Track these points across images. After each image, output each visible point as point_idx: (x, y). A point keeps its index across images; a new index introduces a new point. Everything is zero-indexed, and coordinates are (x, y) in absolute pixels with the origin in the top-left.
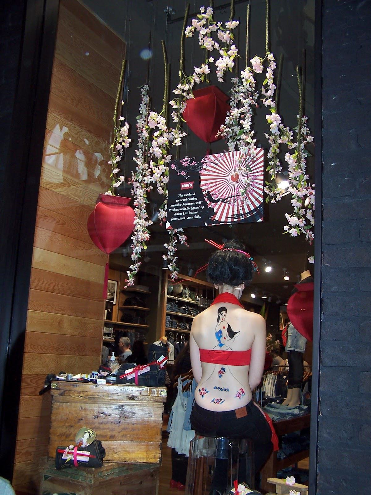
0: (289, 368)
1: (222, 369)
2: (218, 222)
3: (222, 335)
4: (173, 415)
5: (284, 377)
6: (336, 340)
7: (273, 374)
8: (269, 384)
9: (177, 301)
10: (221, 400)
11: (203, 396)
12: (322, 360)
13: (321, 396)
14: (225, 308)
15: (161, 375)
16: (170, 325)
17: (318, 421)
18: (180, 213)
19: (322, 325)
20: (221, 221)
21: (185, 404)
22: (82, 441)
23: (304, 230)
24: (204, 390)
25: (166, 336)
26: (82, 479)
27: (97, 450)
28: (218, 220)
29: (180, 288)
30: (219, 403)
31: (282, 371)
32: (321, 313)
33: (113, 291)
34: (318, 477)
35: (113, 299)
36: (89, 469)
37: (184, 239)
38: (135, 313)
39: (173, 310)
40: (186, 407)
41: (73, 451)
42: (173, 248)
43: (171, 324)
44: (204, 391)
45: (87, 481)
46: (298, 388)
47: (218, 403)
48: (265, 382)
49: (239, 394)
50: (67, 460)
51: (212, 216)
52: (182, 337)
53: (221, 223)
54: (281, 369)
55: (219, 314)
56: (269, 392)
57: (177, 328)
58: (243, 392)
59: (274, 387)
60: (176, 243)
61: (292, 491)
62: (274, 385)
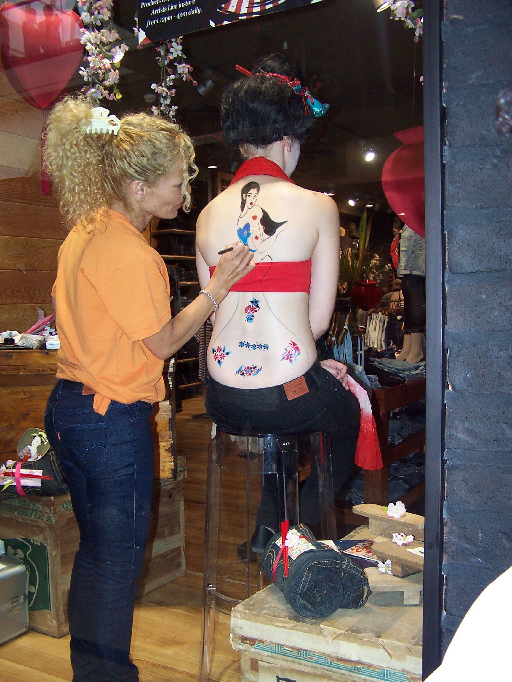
0: (405, 304)
2: (236, 15)
5: (398, 317)
6: (481, 207)
7: (380, 313)
8: (375, 330)
10: (254, 368)
11: (219, 362)
12: (448, 259)
13: (449, 344)
14: (251, 182)
17: (444, 405)
18: (162, 8)
19: (447, 173)
20: (241, 13)
22: (29, 452)
23: (411, 21)
24: (222, 350)
26: (36, 516)
27: (55, 466)
28: (234, 11)
30: (252, 373)
31: (394, 308)
32: (443, 143)
34: (446, 530)
36: (45, 499)
37: (186, 71)
38: (176, 239)
41: (14, 471)
42: (165, 89)
44: (222, 352)
45: (45, 519)
46: (419, 332)
47: (250, 374)
48: (369, 326)
49: (289, 352)
50: (4, 485)
51: (223, 6)
53: (240, 18)
54: (393, 306)
56: (376, 341)
58: (297, 349)
59: (384, 334)
60: (174, 80)
61: (397, 534)
62: (383, 330)
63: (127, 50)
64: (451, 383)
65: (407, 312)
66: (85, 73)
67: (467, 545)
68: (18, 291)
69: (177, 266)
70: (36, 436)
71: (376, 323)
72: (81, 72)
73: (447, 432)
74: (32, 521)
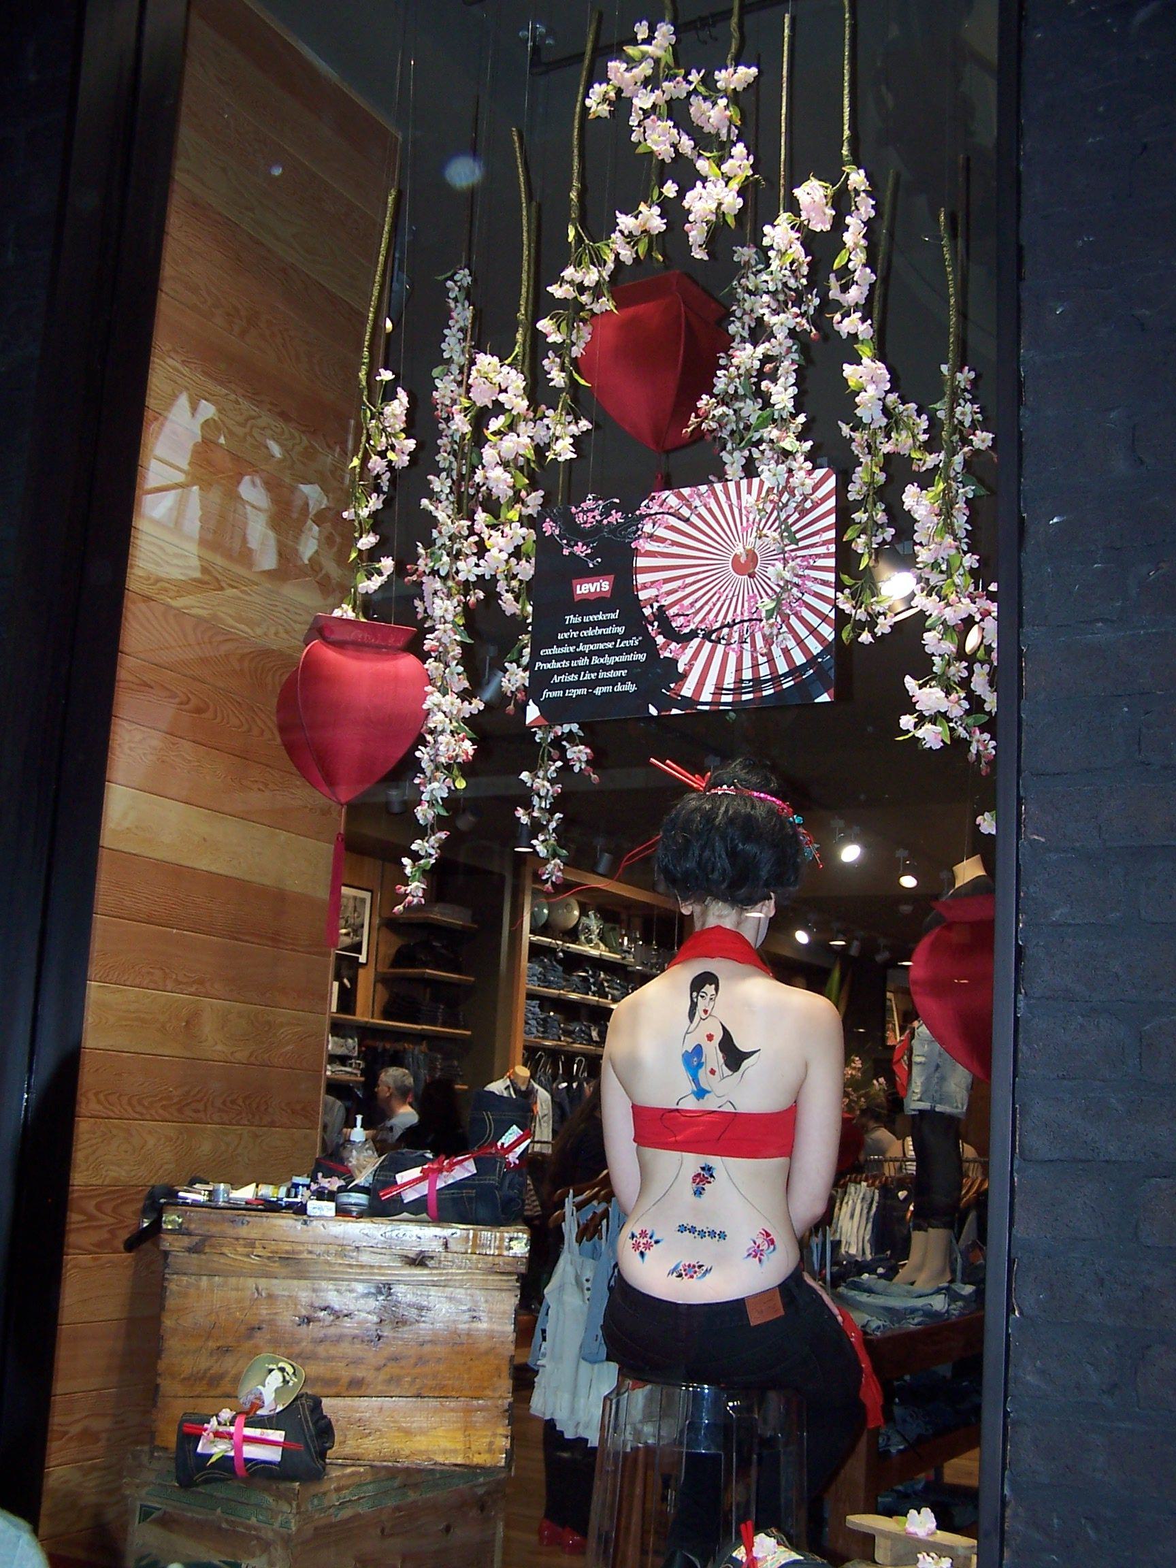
0: (917, 1166)
1: (703, 1169)
2: (691, 702)
3: (703, 1060)
4: (547, 1314)
6: (1064, 1077)
7: (864, 1184)
8: (852, 1216)
9: (561, 954)
10: (700, 1267)
11: (642, 1254)
15: (511, 1186)
16: (538, 1031)
17: (1008, 1335)
18: (570, 674)
21: (587, 1280)
22: (260, 1397)
23: (965, 729)
25: (525, 1065)
28: (689, 695)
29: (572, 910)
31: (893, 1174)
33: (358, 921)
34: (1008, 1512)
35: (357, 948)
36: (283, 1486)
37: (584, 758)
38: (428, 990)
39: (550, 982)
40: (588, 1289)
41: (232, 1429)
42: (547, 785)
43: (544, 1026)
45: (276, 1525)
47: (692, 1277)
48: (840, 1209)
51: (672, 686)
52: (575, 1066)
54: (889, 1170)
55: (695, 994)
56: (853, 1240)
57: (560, 1038)
58: (772, 1242)
59: (870, 1226)
60: (558, 770)
62: (867, 1219)
63: (481, 708)
64: (1018, 1305)
65: (920, 1186)
66: (426, 756)
67: (1037, 1536)
68: (233, 1102)
69: (424, 1047)
70: (273, 1370)
71: (854, 1204)
72: (418, 754)
73: (1011, 1373)
74: (248, 1527)
